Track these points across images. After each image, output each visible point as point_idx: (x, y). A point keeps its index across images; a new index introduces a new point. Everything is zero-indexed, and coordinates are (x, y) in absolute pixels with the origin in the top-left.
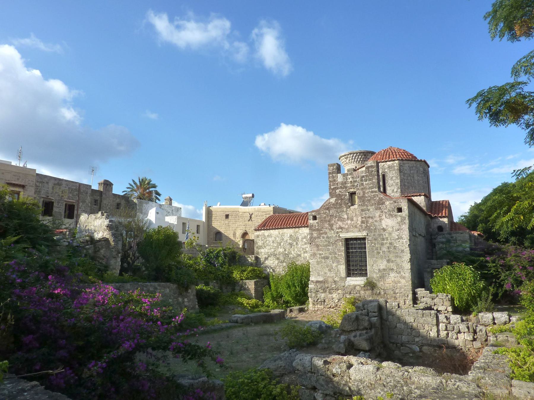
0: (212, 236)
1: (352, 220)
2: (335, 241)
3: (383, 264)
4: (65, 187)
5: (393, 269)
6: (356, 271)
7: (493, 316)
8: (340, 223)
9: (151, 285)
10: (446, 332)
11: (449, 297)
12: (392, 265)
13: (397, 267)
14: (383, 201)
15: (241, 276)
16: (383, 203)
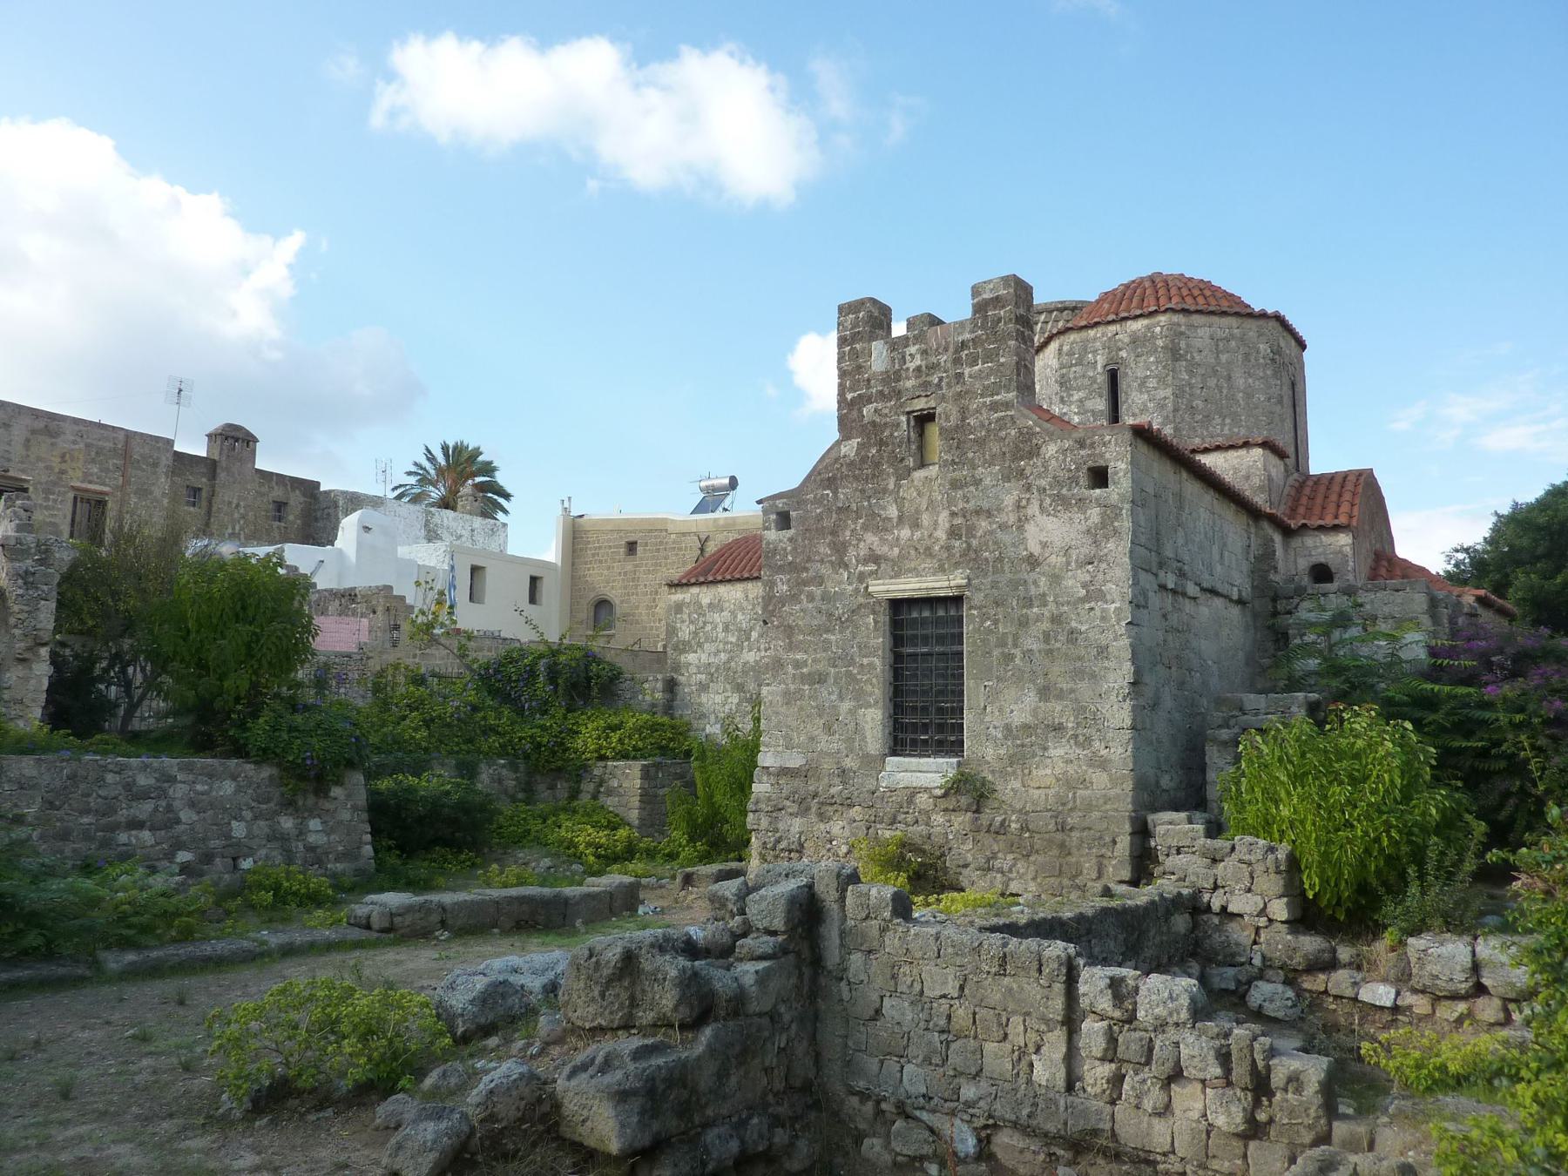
0: (585, 613)
1: (916, 525)
2: (853, 611)
3: (1021, 707)
4: (75, 442)
5: (1058, 728)
6: (923, 734)
7: (1474, 953)
8: (871, 539)
9: (146, 766)
10: (1107, 1069)
11: (1281, 855)
12: (1058, 710)
13: (1076, 718)
14: (1035, 441)
15: (601, 747)
16: (1035, 452)
